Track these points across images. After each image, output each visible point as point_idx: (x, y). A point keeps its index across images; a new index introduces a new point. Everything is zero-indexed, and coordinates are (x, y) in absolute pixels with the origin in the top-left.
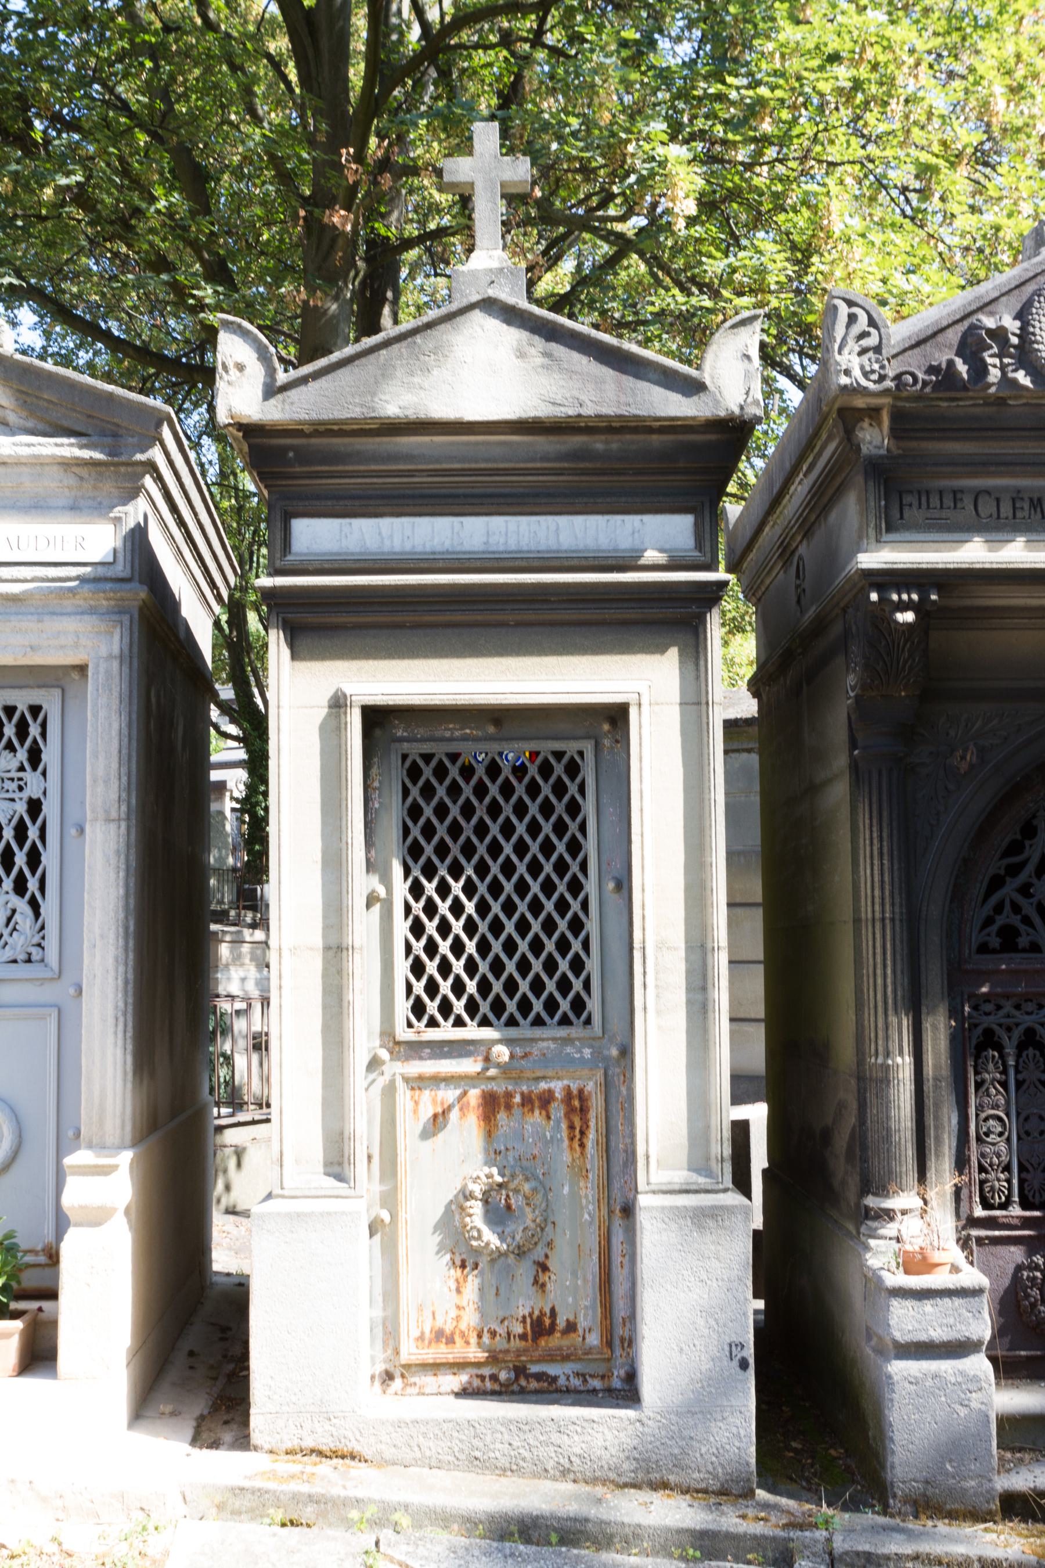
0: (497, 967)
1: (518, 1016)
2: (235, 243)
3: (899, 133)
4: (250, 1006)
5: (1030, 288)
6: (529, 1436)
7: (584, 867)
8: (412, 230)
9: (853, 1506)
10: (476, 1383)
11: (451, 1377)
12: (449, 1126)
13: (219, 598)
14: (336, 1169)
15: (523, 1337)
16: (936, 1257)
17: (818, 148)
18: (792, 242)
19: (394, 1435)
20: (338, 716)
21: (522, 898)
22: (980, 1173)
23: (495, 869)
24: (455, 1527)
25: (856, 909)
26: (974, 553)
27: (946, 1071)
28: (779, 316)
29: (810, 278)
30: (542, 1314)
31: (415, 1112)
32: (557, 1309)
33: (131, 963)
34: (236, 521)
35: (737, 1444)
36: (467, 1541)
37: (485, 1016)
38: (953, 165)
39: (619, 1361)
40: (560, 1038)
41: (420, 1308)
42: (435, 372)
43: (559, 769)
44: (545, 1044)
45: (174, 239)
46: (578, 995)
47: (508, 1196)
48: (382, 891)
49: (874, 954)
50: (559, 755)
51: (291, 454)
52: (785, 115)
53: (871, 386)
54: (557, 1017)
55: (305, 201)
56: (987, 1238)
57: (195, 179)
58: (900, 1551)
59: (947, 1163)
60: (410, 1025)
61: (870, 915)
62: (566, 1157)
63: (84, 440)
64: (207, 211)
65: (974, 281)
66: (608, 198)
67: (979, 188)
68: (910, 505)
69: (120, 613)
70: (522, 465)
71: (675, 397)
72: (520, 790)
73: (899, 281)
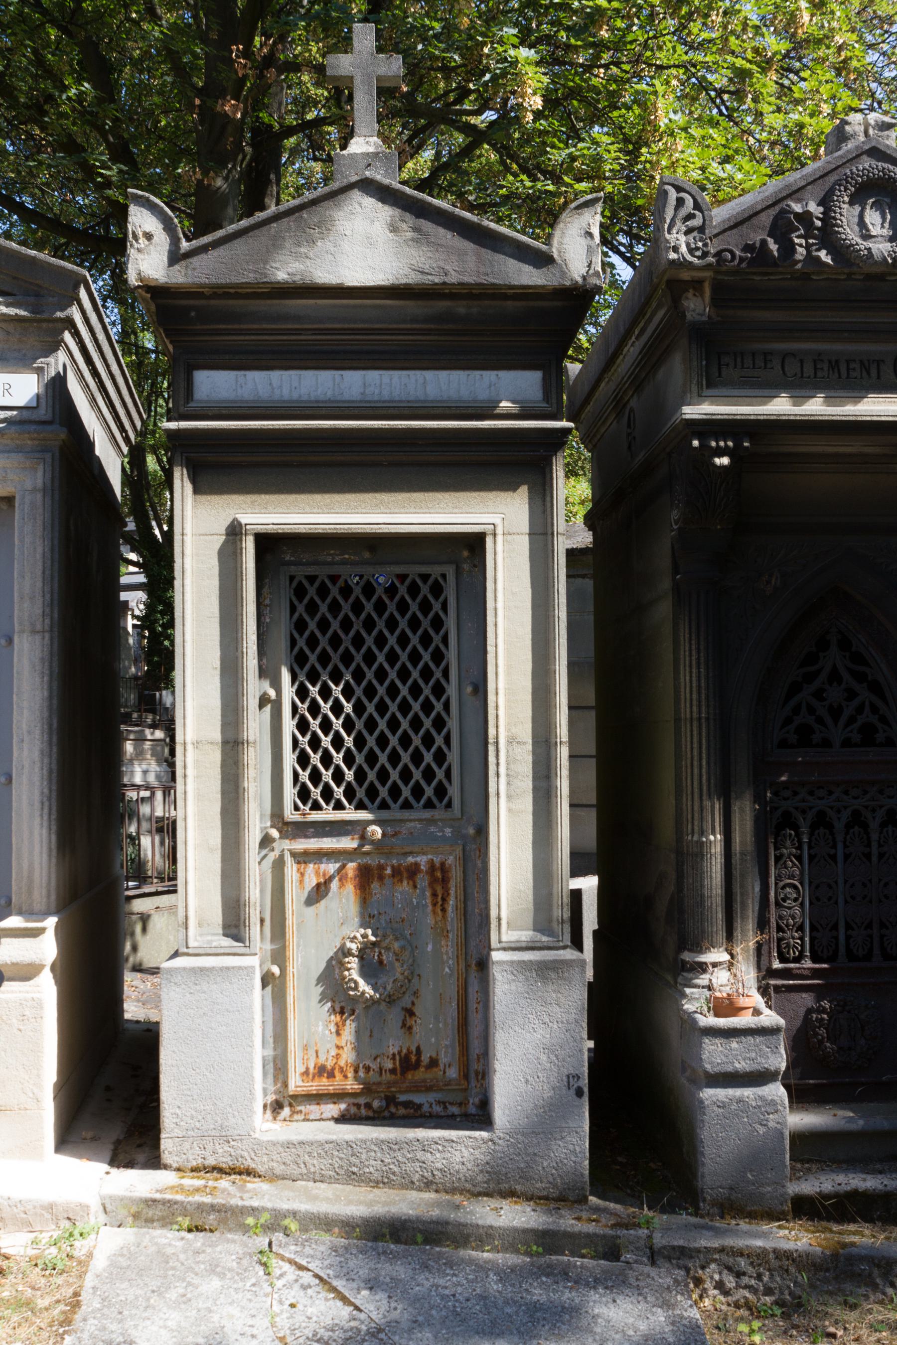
0: (371, 759)
1: (389, 801)
2: (136, 128)
3: (718, 42)
4: (153, 794)
5: (832, 178)
6: (398, 1154)
7: (446, 673)
8: (291, 120)
9: (670, 1209)
10: (353, 1110)
11: (331, 1106)
12: (330, 894)
13: (127, 439)
14: (234, 931)
15: (393, 1071)
16: (742, 1002)
17: (649, 53)
18: (624, 134)
19: (283, 1154)
20: (234, 543)
21: (393, 700)
22: (778, 932)
23: (370, 675)
24: (336, 1230)
25: (677, 710)
26: (781, 406)
27: (750, 847)
28: (612, 200)
29: (640, 166)
30: (409, 1052)
31: (301, 882)
32: (422, 1048)
33: (55, 756)
34: (141, 371)
35: (573, 1159)
36: (346, 1242)
37: (361, 801)
38: (764, 71)
39: (474, 1091)
40: (425, 819)
41: (306, 1048)
42: (319, 244)
43: (425, 590)
44: (412, 824)
45: (83, 124)
46: (440, 782)
47: (380, 953)
48: (272, 693)
49: (692, 748)
50: (425, 577)
51: (193, 314)
52: (619, 24)
53: (695, 261)
54: (422, 802)
55: (200, 92)
56: (783, 986)
57: (100, 70)
58: (709, 1245)
59: (751, 925)
60: (296, 808)
61: (688, 716)
62: (430, 920)
63: (10, 299)
64: (113, 101)
65: (778, 171)
66: (464, 93)
67: (784, 91)
68: (727, 365)
69: (43, 451)
70: (395, 326)
71: (527, 268)
72: (391, 607)
73: (715, 168)
